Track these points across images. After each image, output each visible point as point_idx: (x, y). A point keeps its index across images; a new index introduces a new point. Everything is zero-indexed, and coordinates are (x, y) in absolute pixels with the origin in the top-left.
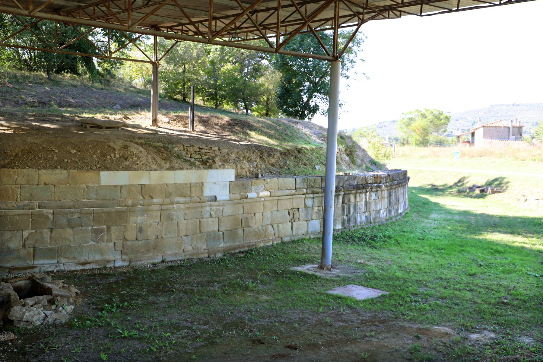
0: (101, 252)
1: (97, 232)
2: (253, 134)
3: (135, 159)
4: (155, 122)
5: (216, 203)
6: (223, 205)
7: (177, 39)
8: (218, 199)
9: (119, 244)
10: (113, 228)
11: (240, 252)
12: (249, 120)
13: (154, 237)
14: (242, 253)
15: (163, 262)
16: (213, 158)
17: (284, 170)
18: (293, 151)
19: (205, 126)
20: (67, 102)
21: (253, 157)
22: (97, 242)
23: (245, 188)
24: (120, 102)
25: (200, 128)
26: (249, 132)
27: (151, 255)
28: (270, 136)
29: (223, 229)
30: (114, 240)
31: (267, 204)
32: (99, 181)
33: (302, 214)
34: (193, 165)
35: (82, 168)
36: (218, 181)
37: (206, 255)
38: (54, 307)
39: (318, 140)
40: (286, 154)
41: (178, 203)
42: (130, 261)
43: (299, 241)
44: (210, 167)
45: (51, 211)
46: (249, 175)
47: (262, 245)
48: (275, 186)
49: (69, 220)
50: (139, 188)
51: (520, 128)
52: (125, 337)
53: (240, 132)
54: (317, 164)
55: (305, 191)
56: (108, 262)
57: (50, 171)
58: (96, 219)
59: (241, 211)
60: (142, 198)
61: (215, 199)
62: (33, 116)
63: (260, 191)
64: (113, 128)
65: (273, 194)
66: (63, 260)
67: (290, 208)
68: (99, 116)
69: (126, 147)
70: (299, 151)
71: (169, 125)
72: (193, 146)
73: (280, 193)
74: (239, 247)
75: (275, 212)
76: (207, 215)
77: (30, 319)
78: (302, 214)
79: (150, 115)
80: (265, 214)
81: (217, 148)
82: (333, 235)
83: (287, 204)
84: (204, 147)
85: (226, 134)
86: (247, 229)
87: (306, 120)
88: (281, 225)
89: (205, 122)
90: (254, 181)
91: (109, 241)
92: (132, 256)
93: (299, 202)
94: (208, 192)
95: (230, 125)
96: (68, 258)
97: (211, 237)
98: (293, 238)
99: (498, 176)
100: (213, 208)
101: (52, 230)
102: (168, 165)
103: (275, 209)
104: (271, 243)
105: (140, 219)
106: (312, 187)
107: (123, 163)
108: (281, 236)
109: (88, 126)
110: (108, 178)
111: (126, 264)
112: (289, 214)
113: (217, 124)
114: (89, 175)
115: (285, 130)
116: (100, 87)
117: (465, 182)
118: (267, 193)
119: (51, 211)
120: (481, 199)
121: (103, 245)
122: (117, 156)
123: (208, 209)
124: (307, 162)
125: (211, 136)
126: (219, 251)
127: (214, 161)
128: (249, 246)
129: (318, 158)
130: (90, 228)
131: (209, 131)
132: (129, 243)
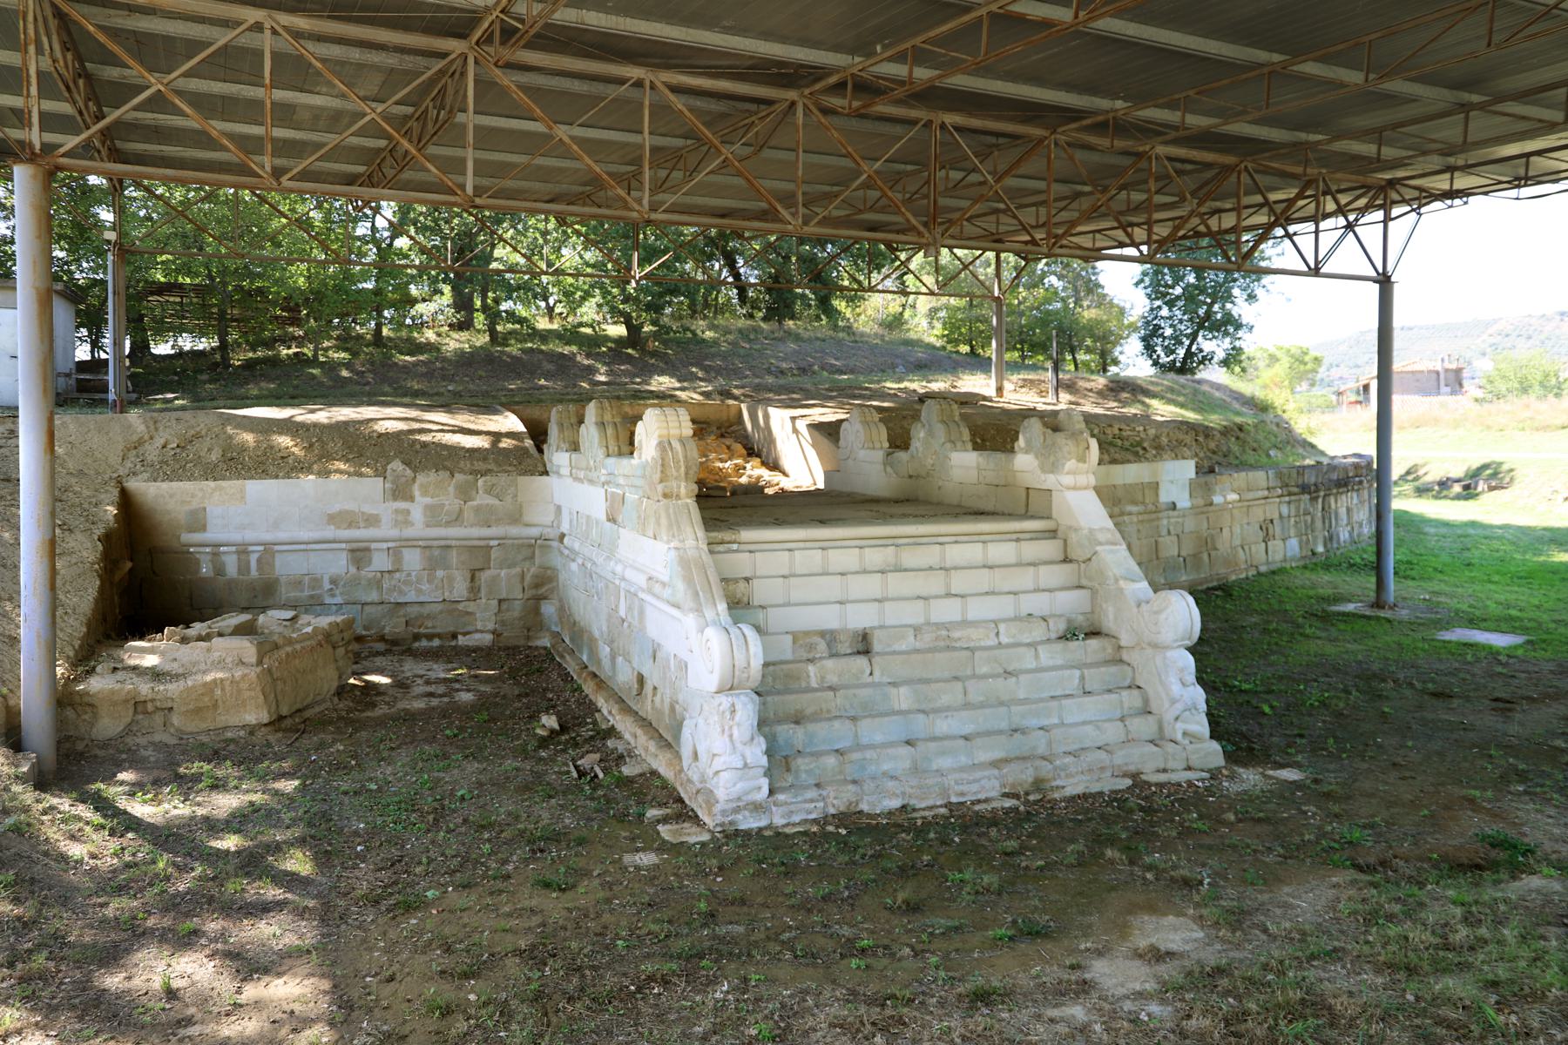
2: (1154, 403)
4: (1000, 390)
23: (1208, 489)
25: (1065, 397)
26: (1147, 400)
28: (1182, 406)
29: (1184, 553)
40: (1226, 431)
41: (1130, 514)
48: (1243, 485)
51: (1458, 371)
59: (1205, 525)
61: (1174, 506)
63: (1226, 494)
70: (1241, 428)
73: (1251, 495)
74: (1206, 580)
76: (1164, 532)
79: (993, 383)
82: (16, 528)
83: (1259, 514)
84: (1123, 426)
86: (1213, 553)
94: (1165, 497)
95: (1112, 390)
99: (1487, 460)
117: (1421, 473)
120: (1462, 503)
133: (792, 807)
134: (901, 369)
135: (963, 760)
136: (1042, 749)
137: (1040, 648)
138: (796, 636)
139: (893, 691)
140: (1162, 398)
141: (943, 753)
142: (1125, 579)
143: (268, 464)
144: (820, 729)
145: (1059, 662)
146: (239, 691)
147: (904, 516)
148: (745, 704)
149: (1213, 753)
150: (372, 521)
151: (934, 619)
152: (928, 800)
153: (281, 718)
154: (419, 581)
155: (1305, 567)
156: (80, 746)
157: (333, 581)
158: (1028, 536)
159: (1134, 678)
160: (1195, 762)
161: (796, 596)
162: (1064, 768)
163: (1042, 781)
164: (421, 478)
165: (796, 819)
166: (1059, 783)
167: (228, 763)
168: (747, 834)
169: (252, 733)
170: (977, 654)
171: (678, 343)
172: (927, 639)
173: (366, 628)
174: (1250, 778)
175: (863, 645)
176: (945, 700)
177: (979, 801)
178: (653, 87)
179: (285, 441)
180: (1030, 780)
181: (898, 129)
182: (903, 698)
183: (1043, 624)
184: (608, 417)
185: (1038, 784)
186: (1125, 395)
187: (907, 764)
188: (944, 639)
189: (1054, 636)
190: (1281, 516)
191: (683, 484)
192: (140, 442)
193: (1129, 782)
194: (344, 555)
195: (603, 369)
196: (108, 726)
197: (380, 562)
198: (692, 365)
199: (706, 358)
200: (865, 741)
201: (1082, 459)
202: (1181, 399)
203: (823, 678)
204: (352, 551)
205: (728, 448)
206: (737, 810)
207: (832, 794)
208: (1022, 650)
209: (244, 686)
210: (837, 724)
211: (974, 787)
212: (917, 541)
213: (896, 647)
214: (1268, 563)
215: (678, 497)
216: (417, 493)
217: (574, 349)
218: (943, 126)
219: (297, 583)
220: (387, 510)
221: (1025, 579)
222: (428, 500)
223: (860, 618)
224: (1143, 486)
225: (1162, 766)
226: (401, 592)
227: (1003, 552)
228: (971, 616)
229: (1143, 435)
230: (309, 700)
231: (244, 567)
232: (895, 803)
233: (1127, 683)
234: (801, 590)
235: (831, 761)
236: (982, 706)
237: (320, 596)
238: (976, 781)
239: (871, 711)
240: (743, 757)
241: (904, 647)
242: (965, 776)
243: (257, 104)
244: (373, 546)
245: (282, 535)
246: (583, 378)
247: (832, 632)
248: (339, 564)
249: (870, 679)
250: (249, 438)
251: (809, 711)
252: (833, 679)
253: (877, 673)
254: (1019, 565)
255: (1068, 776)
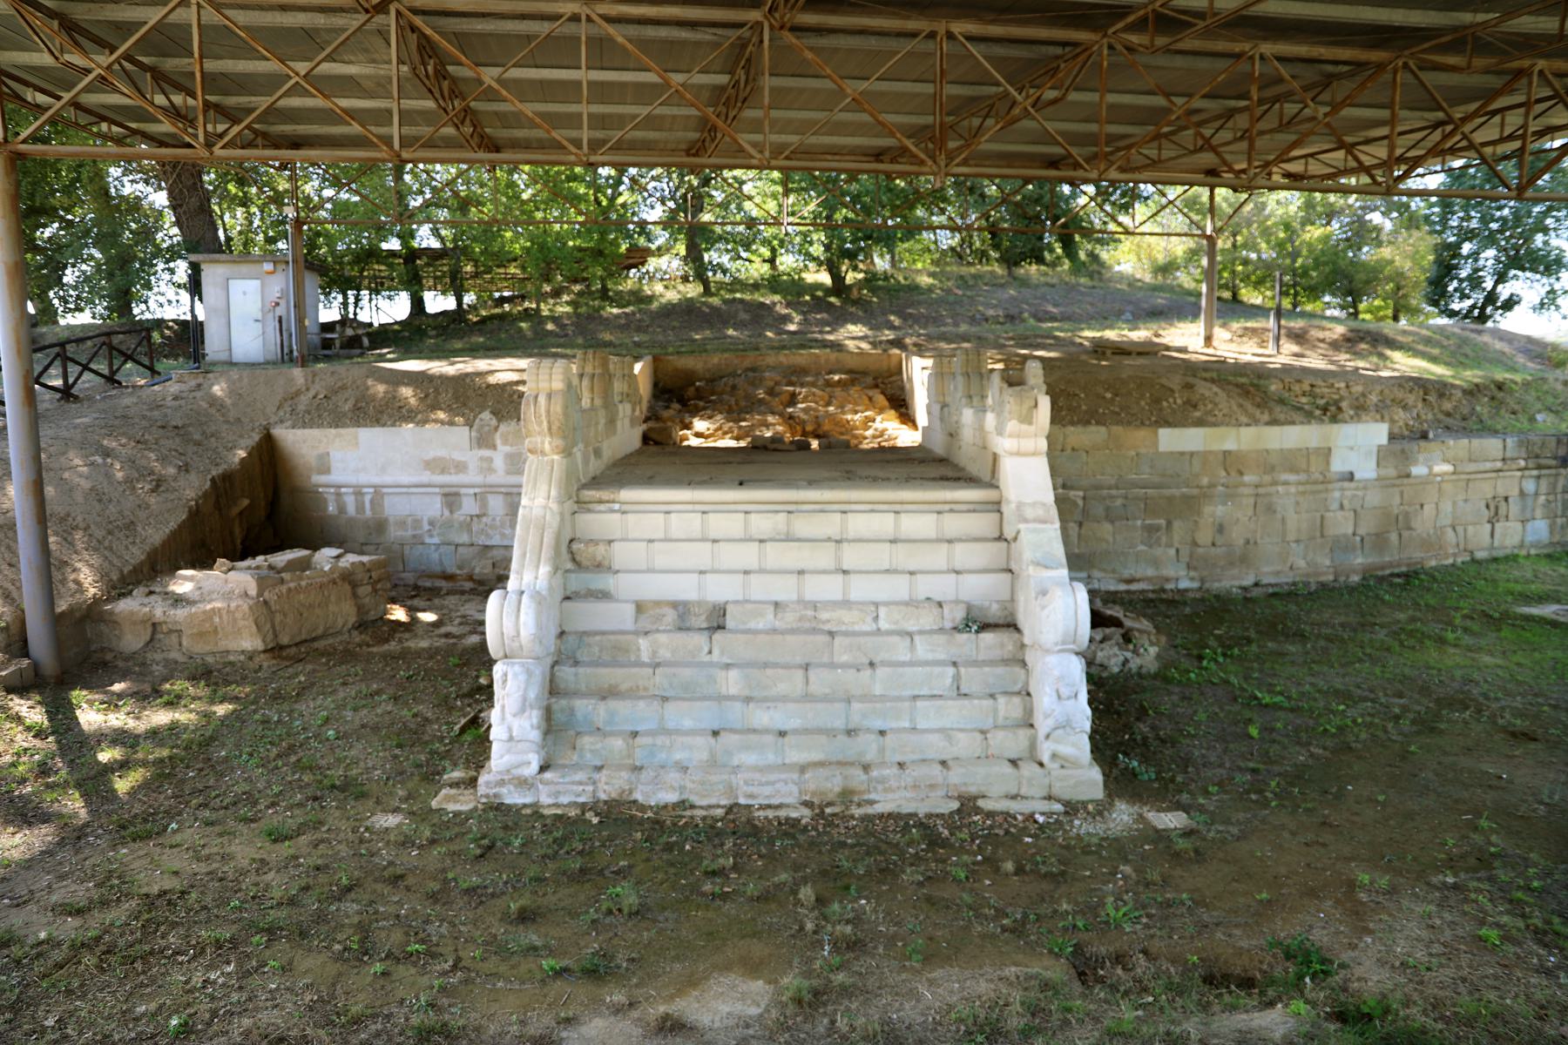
0: (1156, 563)
1: (1151, 530)
2: (1397, 356)
3: (1210, 406)
4: (1208, 340)
5: (1352, 485)
6: (1365, 488)
7: (1553, 200)
8: (1357, 476)
9: (1185, 552)
10: (1177, 524)
11: (1392, 575)
12: (1386, 331)
13: (1242, 542)
14: (1398, 575)
15: (1256, 585)
16: (1336, 403)
17: (1472, 424)
18: (1486, 387)
19: (1298, 343)
20: (1047, 312)
21: (1411, 399)
22: (1150, 546)
23: (1406, 458)
24: (1131, 308)
25: (1289, 347)
26: (1388, 352)
27: (1235, 571)
28: (1433, 359)
29: (1362, 531)
30: (1176, 545)
31: (1447, 487)
32: (1156, 444)
33: (1514, 508)
34: (1309, 417)
35: (1129, 423)
36: (1358, 445)
37: (1331, 578)
38: (1131, 647)
39: (1530, 364)
40: (1473, 392)
41: (1286, 483)
42: (1202, 581)
43: (1507, 558)
44: (1334, 420)
45: (1081, 493)
46: (1406, 433)
47: (1433, 563)
49: (1108, 509)
50: (1221, 457)
52: (1266, 706)
53: (1371, 353)
54: (1539, 412)
55: (1522, 463)
56: (1167, 580)
57: (1080, 429)
58: (1150, 507)
59: (1397, 500)
60: (1223, 473)
61: (1351, 477)
62: (1011, 339)
63: (1435, 464)
64: (1147, 354)
65: (1459, 469)
66: (1096, 574)
67: (1490, 496)
68: (1111, 335)
69: (1189, 386)
70: (1500, 386)
71: (1232, 345)
72: (1299, 381)
73: (1472, 467)
74: (1391, 565)
75: (1461, 504)
76: (1335, 506)
77: (1106, 662)
78: (1514, 508)
80: (1441, 506)
81: (1342, 385)
83: (1486, 489)
84: (1320, 383)
85: (1343, 357)
86: (1406, 534)
87: (1490, 324)
88: (1470, 528)
89: (1299, 337)
90: (1423, 443)
91: (1169, 545)
92: (1205, 573)
93: (1509, 485)
94: (1338, 465)
95: (1348, 340)
96: (1104, 570)
97: (1340, 546)
98: (1495, 554)
100: (1348, 493)
101: (1080, 525)
102: (1266, 417)
103: (1461, 497)
104: (1451, 561)
105: (1220, 510)
106: (1537, 457)
107: (1189, 414)
108: (1470, 547)
109: (1109, 352)
110: (1172, 440)
111: (1196, 585)
112: (1488, 507)
113: (1323, 341)
114: (1142, 434)
115: (1460, 347)
116: (1090, 283)
118: (1448, 468)
119: (1081, 493)
121: (1158, 551)
122: (1179, 401)
123: (1337, 494)
124: (1516, 407)
125: (1315, 361)
126: (1354, 572)
127: (1340, 409)
128: (1408, 565)
129: (1538, 398)
130: (1139, 523)
131: (1308, 353)
132: (1200, 550)
133: (560, 788)
134: (1128, 316)
135: (771, 758)
136: (870, 756)
137: (917, 638)
138: (640, 607)
139: (721, 674)
140: (1409, 349)
141: (747, 748)
142: (1038, 564)
143: (386, 413)
144: (622, 707)
145: (942, 656)
146: (235, 620)
147: (875, 479)
148: (516, 675)
149: (1089, 780)
150: (461, 467)
151: (808, 597)
152: (710, 797)
153: (282, 648)
154: (503, 525)
155: (1549, 556)
156: (109, 657)
157: (431, 523)
158: (964, 507)
159: (1027, 683)
160: (1056, 791)
161: (660, 561)
162: (882, 780)
163: (852, 792)
164: (503, 428)
165: (564, 800)
166: (872, 796)
167: (203, 683)
168: (509, 807)
169: (251, 658)
170: (838, 640)
171: (888, 290)
172: (789, 619)
173: (460, 568)
174: (1123, 815)
175: (717, 621)
176: (782, 688)
177: (769, 806)
178: (589, 19)
179: (406, 392)
180: (837, 789)
181: (892, 44)
182: (732, 682)
183: (936, 610)
184: (589, 369)
185: (847, 795)
186: (1363, 346)
187: (705, 756)
188: (812, 622)
189: (948, 625)
190: (1522, 493)
191: (548, 439)
192: (298, 393)
193: (955, 805)
194: (438, 499)
195: (797, 318)
196: (132, 641)
197: (469, 507)
198: (892, 313)
199: (912, 305)
200: (671, 725)
201: (1027, 419)
202: (1436, 351)
203: (654, 653)
204: (445, 495)
205: (870, 399)
206: (502, 783)
207: (604, 779)
208: (896, 639)
209: (238, 615)
210: (641, 704)
211: (767, 790)
212: (822, 508)
213: (752, 625)
214: (1492, 547)
215: (543, 453)
216: (498, 442)
217: (777, 298)
218: (950, 36)
219: (402, 524)
220: (472, 457)
221: (938, 557)
222: (508, 449)
223: (720, 590)
224: (1308, 453)
225: (1014, 791)
226: (487, 535)
227: (920, 524)
228: (854, 596)
229: (1343, 393)
230: (320, 631)
231: (360, 507)
232: (672, 797)
233: (1017, 688)
234: (664, 556)
235: (618, 743)
236: (826, 699)
237: (421, 536)
238: (768, 783)
239: (689, 693)
240: (510, 729)
241: (761, 626)
242: (757, 776)
243: (577, 84)
244: (463, 491)
245: (388, 479)
246: (770, 327)
247: (685, 604)
248: (433, 508)
249: (707, 659)
250: (381, 388)
251: (624, 687)
252: (665, 654)
253: (716, 652)
254: (939, 540)
255: (886, 790)
